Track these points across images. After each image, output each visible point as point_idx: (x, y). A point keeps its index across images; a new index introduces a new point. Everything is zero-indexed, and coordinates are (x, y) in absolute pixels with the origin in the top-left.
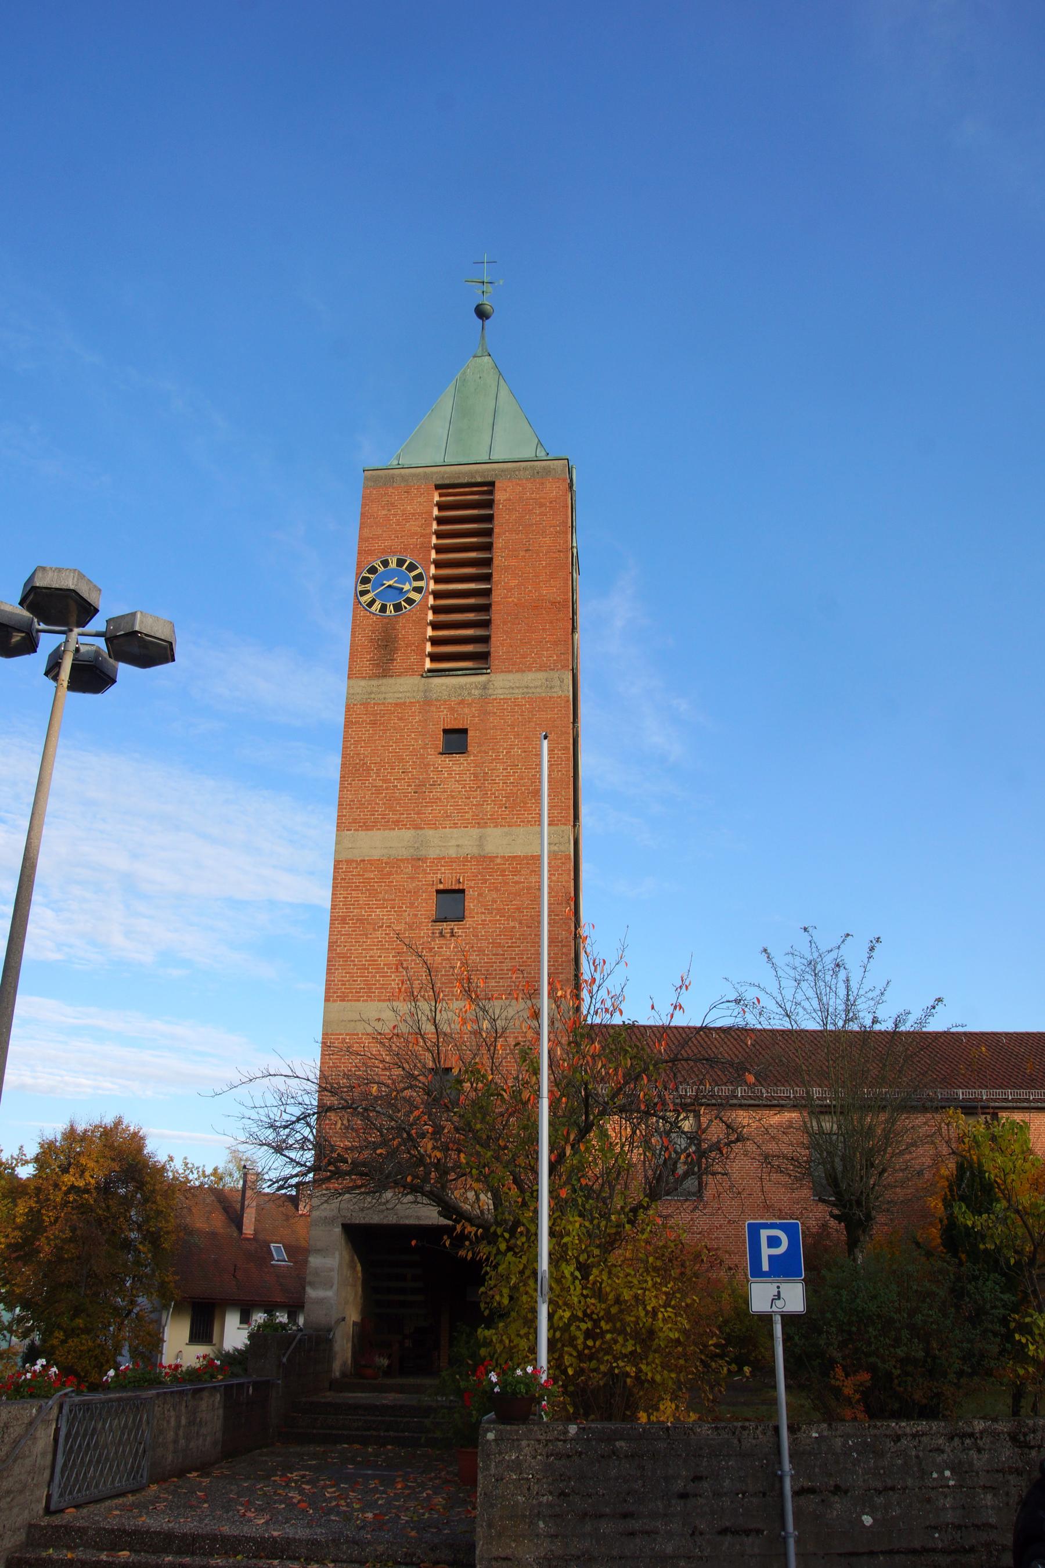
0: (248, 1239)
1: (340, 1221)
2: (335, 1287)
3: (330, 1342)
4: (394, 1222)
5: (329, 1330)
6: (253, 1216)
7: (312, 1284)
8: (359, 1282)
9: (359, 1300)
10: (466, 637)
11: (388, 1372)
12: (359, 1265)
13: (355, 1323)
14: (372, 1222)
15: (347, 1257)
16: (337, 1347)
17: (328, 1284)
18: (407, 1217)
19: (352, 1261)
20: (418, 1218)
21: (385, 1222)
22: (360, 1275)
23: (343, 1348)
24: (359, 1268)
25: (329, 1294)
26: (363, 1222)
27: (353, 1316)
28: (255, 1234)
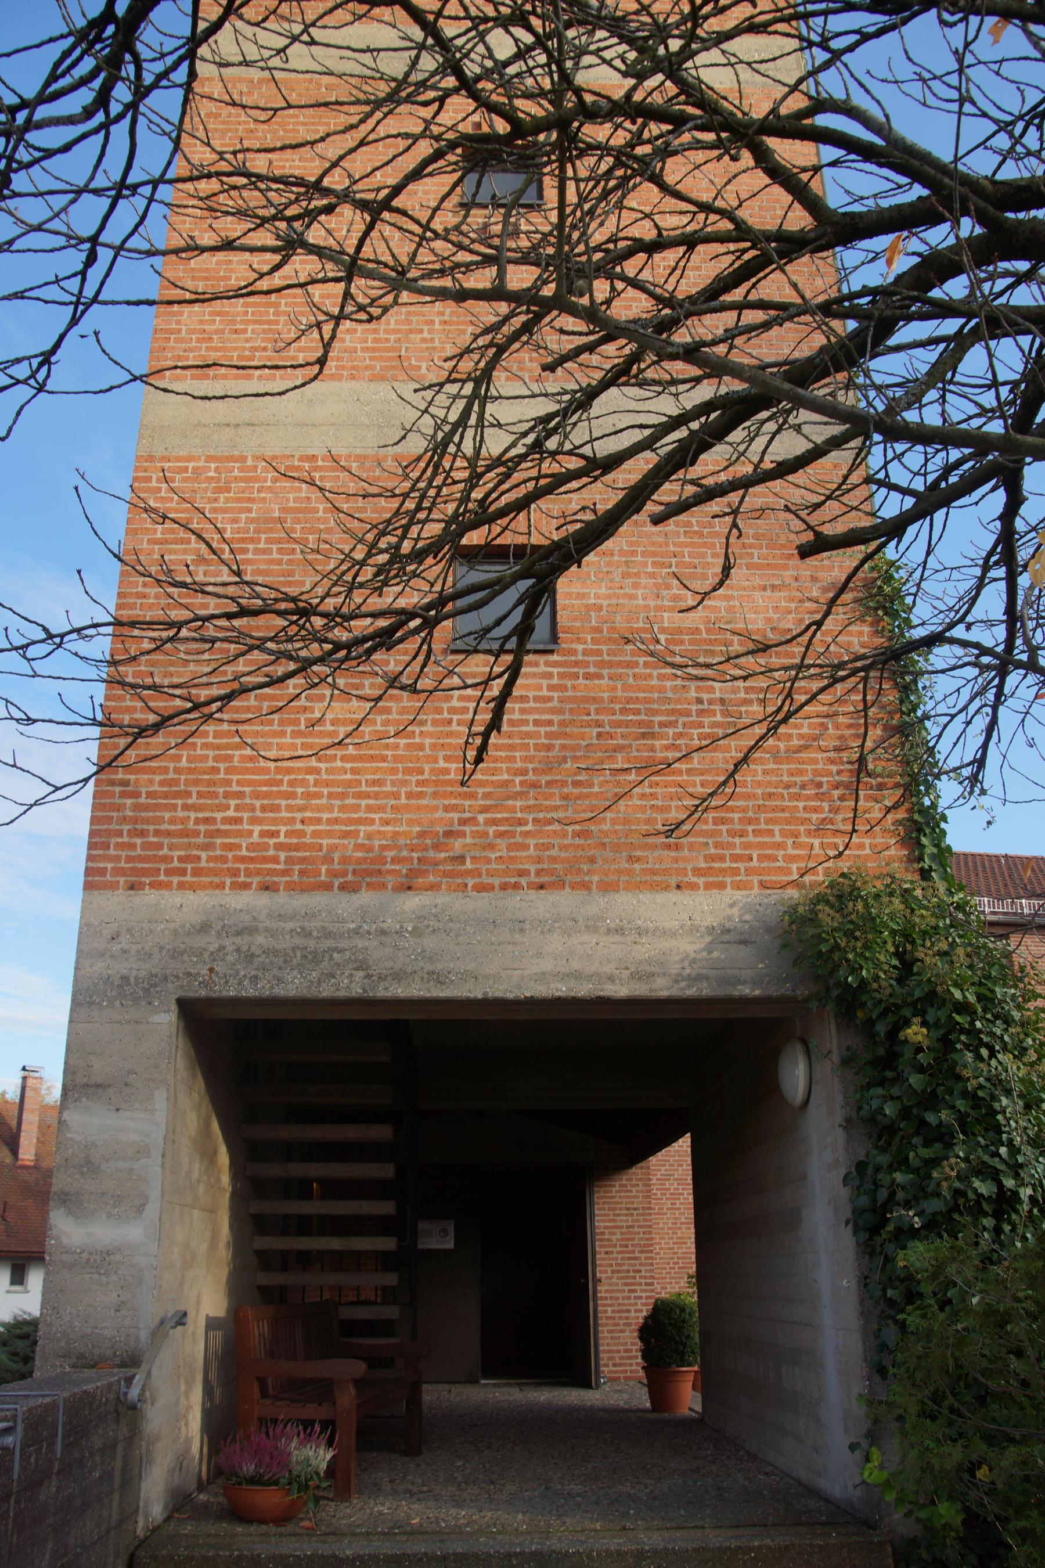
0: (27, 1167)
1: (173, 991)
2: (152, 1210)
3: (127, 1412)
4: (356, 991)
5: (132, 1361)
6: (35, 1135)
7: (69, 1201)
8: (225, 1200)
9: (224, 1253)
10: (199, 931)
11: (340, 1481)
12: (223, 1149)
13: (212, 1324)
14: (280, 992)
15: (192, 1121)
16: (155, 1418)
17: (127, 1202)
18: (398, 976)
19: (205, 1131)
20: (436, 977)
21: (326, 991)
22: (226, 1179)
23: (177, 1416)
24: (224, 1158)
25: (133, 1232)
26: (249, 991)
27: (209, 1298)
28: (38, 1159)
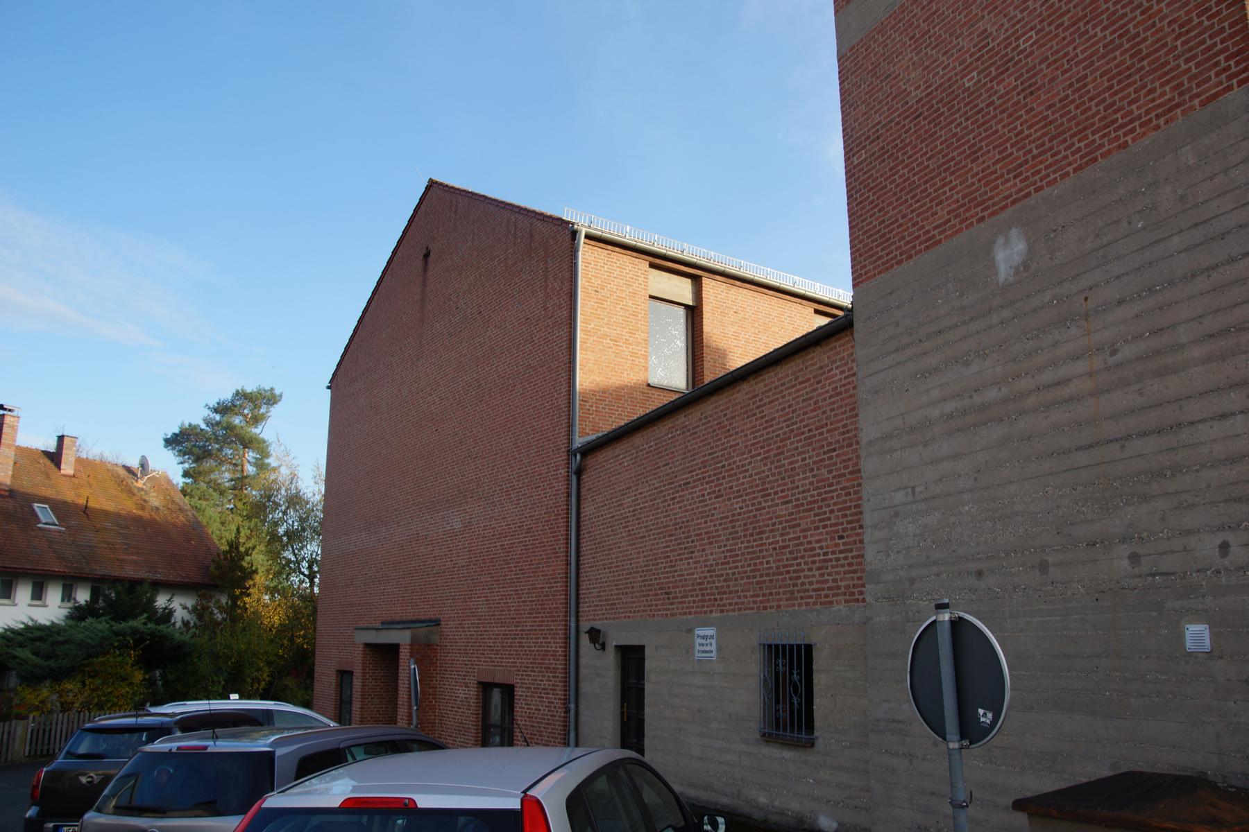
26: (797, 336)
